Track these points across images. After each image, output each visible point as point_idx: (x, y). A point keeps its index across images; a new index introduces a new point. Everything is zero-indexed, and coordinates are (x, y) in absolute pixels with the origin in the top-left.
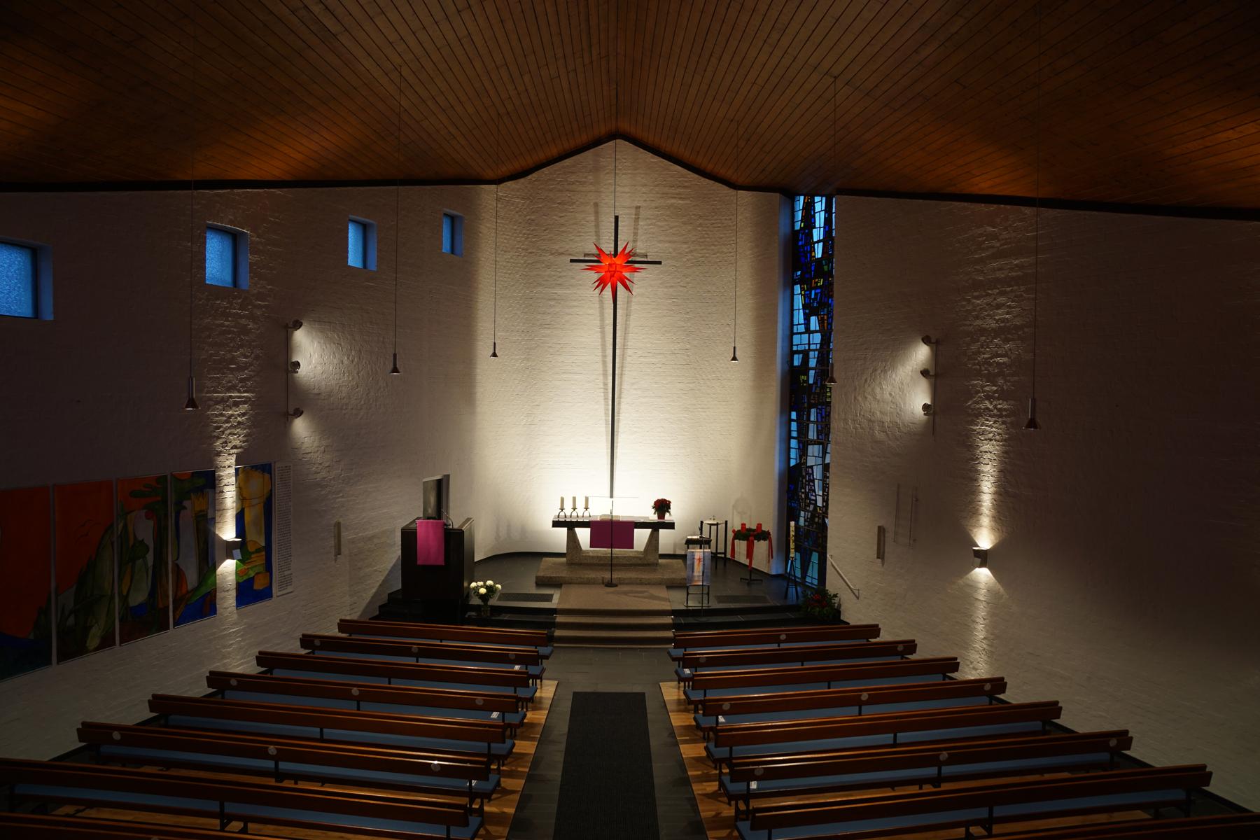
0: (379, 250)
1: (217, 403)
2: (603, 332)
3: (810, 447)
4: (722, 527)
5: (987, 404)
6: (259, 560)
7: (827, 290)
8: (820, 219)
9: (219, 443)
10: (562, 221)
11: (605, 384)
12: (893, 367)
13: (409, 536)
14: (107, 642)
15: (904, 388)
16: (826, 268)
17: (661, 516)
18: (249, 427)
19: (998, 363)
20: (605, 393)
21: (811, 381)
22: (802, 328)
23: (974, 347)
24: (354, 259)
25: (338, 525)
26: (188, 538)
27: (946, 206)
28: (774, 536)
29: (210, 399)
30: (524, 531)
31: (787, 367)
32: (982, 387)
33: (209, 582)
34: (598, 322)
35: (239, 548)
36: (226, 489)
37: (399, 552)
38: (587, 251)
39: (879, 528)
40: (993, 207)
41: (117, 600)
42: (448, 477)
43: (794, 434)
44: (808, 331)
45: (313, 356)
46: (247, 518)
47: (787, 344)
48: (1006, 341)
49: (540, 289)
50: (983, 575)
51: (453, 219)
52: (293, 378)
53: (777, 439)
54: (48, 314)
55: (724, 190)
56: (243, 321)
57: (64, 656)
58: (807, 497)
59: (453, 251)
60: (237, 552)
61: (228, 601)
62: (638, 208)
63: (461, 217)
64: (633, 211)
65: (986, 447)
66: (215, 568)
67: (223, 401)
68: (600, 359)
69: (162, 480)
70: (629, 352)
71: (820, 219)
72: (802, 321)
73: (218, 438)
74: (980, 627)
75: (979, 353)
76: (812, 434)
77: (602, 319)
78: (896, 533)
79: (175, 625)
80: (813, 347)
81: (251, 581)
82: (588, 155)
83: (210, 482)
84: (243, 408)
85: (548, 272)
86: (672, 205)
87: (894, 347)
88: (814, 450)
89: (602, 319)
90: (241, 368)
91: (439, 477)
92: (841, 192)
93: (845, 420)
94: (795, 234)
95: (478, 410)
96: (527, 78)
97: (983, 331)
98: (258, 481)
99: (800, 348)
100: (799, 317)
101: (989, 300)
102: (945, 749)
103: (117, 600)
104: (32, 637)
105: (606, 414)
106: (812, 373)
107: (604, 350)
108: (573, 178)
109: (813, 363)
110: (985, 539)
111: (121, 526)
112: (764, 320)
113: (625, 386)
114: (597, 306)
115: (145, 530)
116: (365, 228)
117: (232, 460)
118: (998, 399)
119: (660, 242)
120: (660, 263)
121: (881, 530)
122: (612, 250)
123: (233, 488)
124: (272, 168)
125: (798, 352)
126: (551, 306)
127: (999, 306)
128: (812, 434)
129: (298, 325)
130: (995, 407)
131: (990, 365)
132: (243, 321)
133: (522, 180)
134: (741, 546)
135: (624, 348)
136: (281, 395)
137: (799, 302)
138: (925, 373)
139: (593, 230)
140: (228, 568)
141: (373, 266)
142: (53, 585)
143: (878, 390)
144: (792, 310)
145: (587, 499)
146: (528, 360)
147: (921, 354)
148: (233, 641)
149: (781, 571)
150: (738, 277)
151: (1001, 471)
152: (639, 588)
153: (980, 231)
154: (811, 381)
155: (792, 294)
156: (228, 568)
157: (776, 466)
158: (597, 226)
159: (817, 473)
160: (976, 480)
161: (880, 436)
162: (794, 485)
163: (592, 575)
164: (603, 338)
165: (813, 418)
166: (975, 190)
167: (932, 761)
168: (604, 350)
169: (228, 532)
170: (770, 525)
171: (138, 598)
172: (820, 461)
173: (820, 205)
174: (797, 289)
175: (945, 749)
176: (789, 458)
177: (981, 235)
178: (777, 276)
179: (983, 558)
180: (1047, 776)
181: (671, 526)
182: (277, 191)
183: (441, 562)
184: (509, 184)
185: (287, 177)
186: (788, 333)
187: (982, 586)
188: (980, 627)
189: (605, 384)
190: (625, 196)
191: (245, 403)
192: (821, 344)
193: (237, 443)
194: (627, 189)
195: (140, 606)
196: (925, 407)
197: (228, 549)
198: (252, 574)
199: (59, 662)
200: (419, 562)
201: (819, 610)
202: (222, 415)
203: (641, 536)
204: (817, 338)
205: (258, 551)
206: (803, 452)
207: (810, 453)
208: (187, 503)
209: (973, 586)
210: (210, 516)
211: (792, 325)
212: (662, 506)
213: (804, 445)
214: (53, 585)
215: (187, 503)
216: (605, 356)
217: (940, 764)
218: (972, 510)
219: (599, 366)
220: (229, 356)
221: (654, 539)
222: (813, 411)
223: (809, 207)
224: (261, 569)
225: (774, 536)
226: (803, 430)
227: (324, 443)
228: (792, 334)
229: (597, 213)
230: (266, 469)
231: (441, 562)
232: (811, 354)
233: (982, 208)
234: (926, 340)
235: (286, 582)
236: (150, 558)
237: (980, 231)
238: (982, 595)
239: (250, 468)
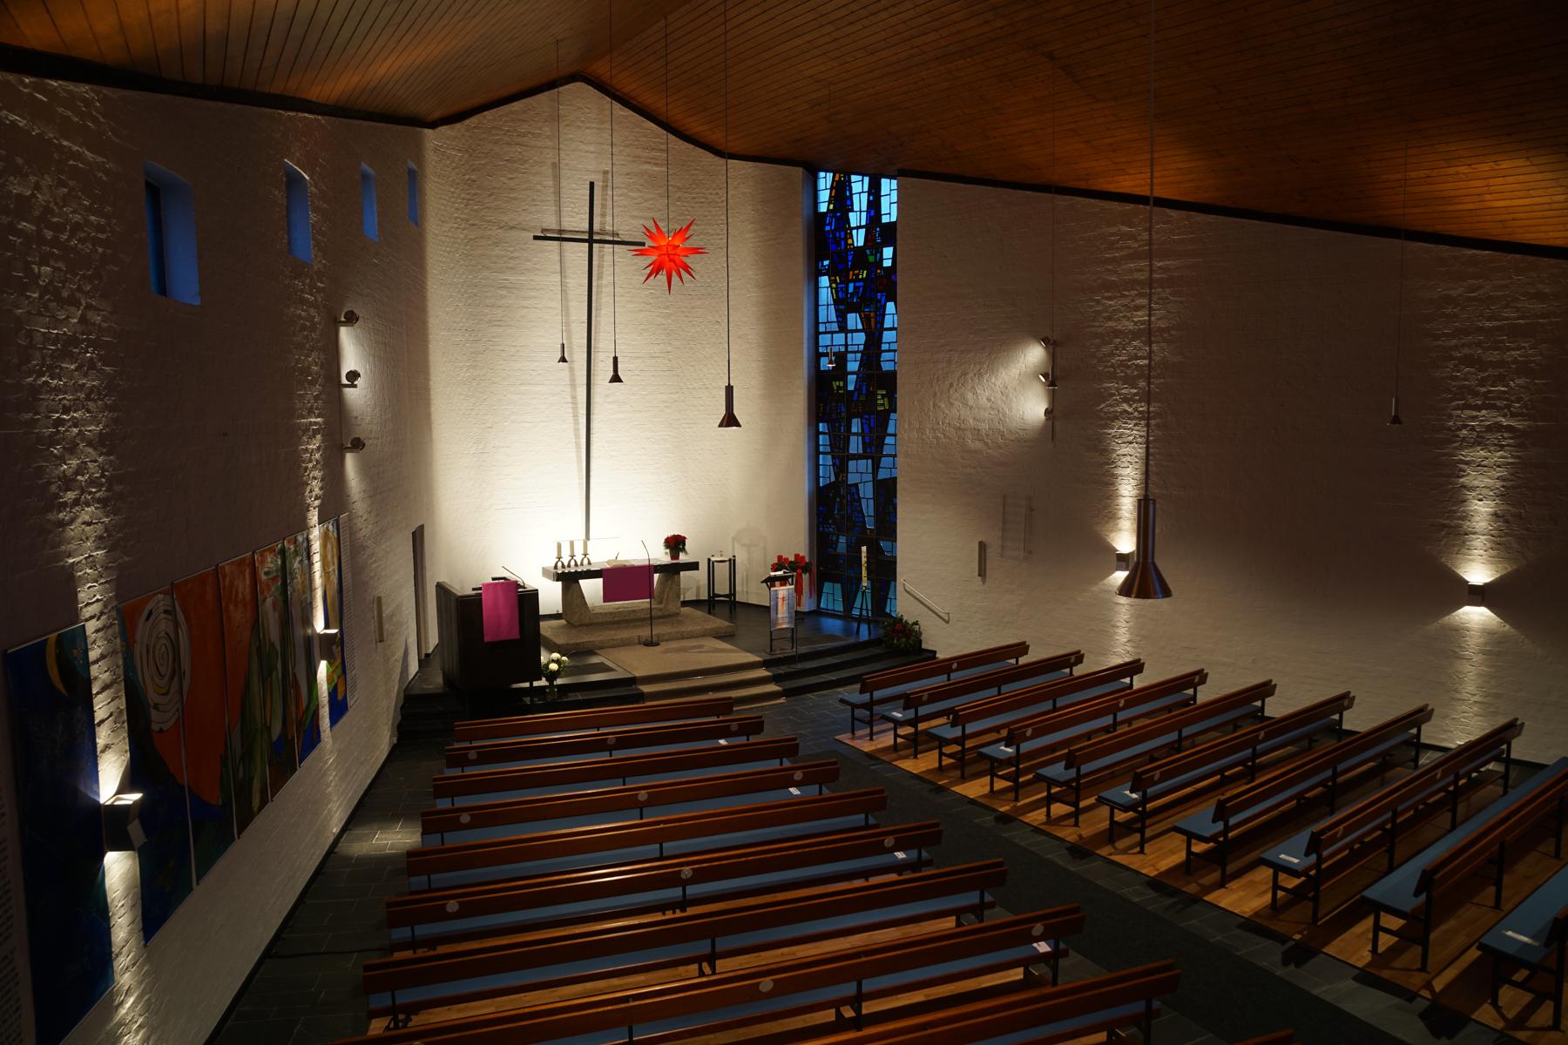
10: (512, 184)
12: (992, 369)
16: (871, 259)
17: (675, 556)
21: (851, 387)
23: (1106, 349)
27: (1062, 201)
38: (545, 226)
40: (1129, 207)
55: (709, 157)
65: (1125, 450)
71: (860, 201)
75: (1112, 354)
76: (855, 445)
78: (1003, 548)
82: (543, 98)
85: (497, 251)
87: (995, 342)
94: (819, 218)
97: (1117, 333)
100: (828, 313)
101: (1126, 301)
102: (688, 864)
106: (852, 379)
108: (524, 128)
109: (853, 366)
112: (775, 316)
118: (1140, 401)
119: (633, 217)
121: (983, 547)
122: (586, 226)
126: (503, 297)
127: (1137, 308)
128: (855, 445)
130: (1136, 409)
131: (1128, 367)
133: (458, 126)
137: (825, 295)
139: (552, 198)
143: (970, 395)
144: (817, 305)
147: (1034, 355)
149: (814, 607)
152: (693, 643)
153: (1111, 230)
154: (851, 387)
158: (558, 193)
161: (973, 444)
163: (624, 634)
165: (854, 430)
167: (673, 880)
172: (870, 477)
174: (824, 281)
175: (688, 864)
176: (818, 478)
177: (1113, 234)
178: (799, 267)
180: (874, 880)
183: (515, 634)
184: (443, 129)
192: (865, 345)
194: (592, 148)
201: (901, 645)
204: (860, 338)
206: (841, 468)
211: (817, 323)
212: (675, 544)
217: (684, 883)
218: (1105, 509)
228: (817, 333)
229: (557, 178)
231: (515, 634)
233: (1115, 206)
234: (1046, 341)
237: (1111, 230)
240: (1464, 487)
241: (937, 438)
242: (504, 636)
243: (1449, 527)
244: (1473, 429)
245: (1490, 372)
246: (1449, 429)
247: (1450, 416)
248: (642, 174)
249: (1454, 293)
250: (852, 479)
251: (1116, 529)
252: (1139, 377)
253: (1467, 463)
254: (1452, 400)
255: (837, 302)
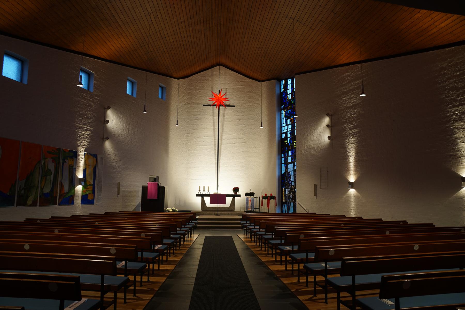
0: (137, 91)
1: (80, 128)
2: (214, 131)
3: (289, 165)
4: (258, 199)
5: (350, 132)
6: (90, 188)
7: (293, 110)
8: (290, 86)
9: (79, 142)
10: (200, 93)
11: (215, 149)
12: (317, 128)
13: (144, 189)
14: (34, 203)
15: (322, 134)
17: (236, 193)
18: (90, 140)
19: (353, 117)
20: (215, 153)
21: (288, 142)
22: (285, 125)
23: (344, 114)
24: (128, 92)
25: (119, 183)
26: (66, 173)
28: (277, 197)
29: (77, 126)
30: (185, 203)
31: (280, 139)
32: (348, 126)
33: (73, 191)
34: (213, 128)
35: (83, 181)
36: (80, 159)
37: (141, 200)
39: (315, 185)
40: (347, 67)
41: (39, 189)
42: (158, 177)
43: (283, 162)
44: (287, 125)
45: (113, 121)
46: (87, 172)
47: (279, 131)
48: (355, 109)
49: (192, 116)
50: (352, 191)
51: (162, 88)
52: (106, 126)
53: (277, 164)
54: (25, 81)
56: (90, 102)
57: (19, 205)
58: (288, 183)
59: (162, 98)
60: (83, 183)
61: (78, 200)
62: (227, 88)
63: (165, 88)
64: (225, 90)
66: (74, 187)
67: (81, 128)
68: (213, 140)
69: (59, 150)
70: (224, 138)
71: (290, 86)
72: (284, 122)
73: (79, 140)
74: (353, 211)
75: (346, 115)
76: (289, 160)
77: (214, 126)
78: (321, 186)
79: (59, 204)
80: (288, 130)
81: (87, 195)
82: (210, 70)
83: (75, 155)
84: (88, 132)
85: (195, 110)
86: (238, 88)
87: (317, 120)
88: (290, 166)
89: (214, 126)
90: (89, 118)
91: (155, 177)
92: (296, 74)
93: (301, 151)
94: (281, 93)
95: (170, 156)
96: (191, 28)
97: (347, 108)
98: (92, 160)
99: (285, 131)
101: (348, 97)
103: (39, 189)
104: (8, 194)
105: (215, 160)
106: (289, 139)
107: (215, 137)
109: (289, 136)
110: (352, 178)
111: (43, 162)
113: (222, 150)
114: (212, 122)
115: (51, 166)
116: (133, 83)
117: (83, 150)
120: (234, 106)
121: (315, 186)
123: (83, 160)
124: (103, 52)
125: (284, 133)
126: (196, 122)
127: (352, 98)
128: (289, 160)
129: (109, 108)
131: (350, 118)
132: (90, 102)
133: (186, 79)
134: (265, 201)
135: (222, 136)
136: (101, 133)
137: (283, 116)
138: (328, 126)
140: (79, 188)
141: (135, 95)
142: (18, 177)
143: (312, 137)
144: (281, 119)
145: (209, 187)
146: (187, 140)
147: (327, 120)
148: (79, 209)
149: (280, 212)
150: (262, 109)
151: (356, 153)
153: (344, 75)
154: (288, 142)
155: (281, 114)
156: (79, 188)
157: (277, 174)
159: (292, 174)
160: (348, 159)
161: (313, 153)
162: (284, 180)
164: (214, 133)
166: (341, 62)
168: (215, 137)
169: (80, 175)
170: (275, 194)
171: (47, 190)
173: (289, 82)
174: (283, 111)
176: (281, 171)
177: (344, 77)
178: (275, 108)
179: (352, 185)
181: (239, 196)
182: (105, 62)
183: (156, 197)
184: (182, 80)
185: (108, 58)
186: (280, 127)
187: (352, 196)
188: (353, 211)
189: (215, 149)
190: (222, 82)
191: (89, 131)
193: (85, 144)
194: (223, 82)
195: (47, 193)
196: (329, 137)
197: (80, 181)
198: (87, 193)
199: (17, 206)
200: (148, 198)
202: (81, 133)
203: (229, 200)
204: (290, 127)
205: (90, 185)
206: (286, 168)
207: (289, 167)
208: (66, 160)
209: (349, 197)
210: (74, 167)
211: (281, 124)
212: (236, 190)
213: (287, 164)
214: (18, 177)
215: (66, 160)
216: (215, 139)
218: (347, 169)
219: (213, 143)
220: (84, 113)
221: (233, 201)
222: (290, 152)
223: (286, 84)
224: (91, 192)
225: (277, 197)
226: (286, 159)
227: (115, 153)
228: (281, 127)
230: (95, 156)
231: (156, 197)
232: (288, 133)
233: (344, 68)
234: (328, 115)
235: (99, 199)
236: (52, 176)
237: (344, 75)
238: (352, 199)
239: (88, 155)
240: (456, 138)
241: (305, 152)
242: (153, 198)
243: (453, 155)
244: (457, 115)
245: (461, 91)
246: (448, 116)
247: (448, 111)
248: (237, 88)
249: (444, 66)
250: (289, 170)
251: (350, 174)
252: (353, 121)
253: (456, 128)
254: (448, 105)
255: (285, 117)
